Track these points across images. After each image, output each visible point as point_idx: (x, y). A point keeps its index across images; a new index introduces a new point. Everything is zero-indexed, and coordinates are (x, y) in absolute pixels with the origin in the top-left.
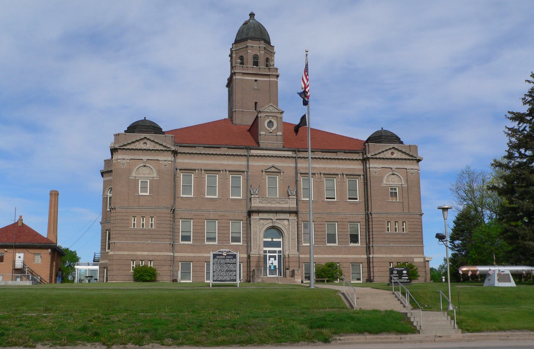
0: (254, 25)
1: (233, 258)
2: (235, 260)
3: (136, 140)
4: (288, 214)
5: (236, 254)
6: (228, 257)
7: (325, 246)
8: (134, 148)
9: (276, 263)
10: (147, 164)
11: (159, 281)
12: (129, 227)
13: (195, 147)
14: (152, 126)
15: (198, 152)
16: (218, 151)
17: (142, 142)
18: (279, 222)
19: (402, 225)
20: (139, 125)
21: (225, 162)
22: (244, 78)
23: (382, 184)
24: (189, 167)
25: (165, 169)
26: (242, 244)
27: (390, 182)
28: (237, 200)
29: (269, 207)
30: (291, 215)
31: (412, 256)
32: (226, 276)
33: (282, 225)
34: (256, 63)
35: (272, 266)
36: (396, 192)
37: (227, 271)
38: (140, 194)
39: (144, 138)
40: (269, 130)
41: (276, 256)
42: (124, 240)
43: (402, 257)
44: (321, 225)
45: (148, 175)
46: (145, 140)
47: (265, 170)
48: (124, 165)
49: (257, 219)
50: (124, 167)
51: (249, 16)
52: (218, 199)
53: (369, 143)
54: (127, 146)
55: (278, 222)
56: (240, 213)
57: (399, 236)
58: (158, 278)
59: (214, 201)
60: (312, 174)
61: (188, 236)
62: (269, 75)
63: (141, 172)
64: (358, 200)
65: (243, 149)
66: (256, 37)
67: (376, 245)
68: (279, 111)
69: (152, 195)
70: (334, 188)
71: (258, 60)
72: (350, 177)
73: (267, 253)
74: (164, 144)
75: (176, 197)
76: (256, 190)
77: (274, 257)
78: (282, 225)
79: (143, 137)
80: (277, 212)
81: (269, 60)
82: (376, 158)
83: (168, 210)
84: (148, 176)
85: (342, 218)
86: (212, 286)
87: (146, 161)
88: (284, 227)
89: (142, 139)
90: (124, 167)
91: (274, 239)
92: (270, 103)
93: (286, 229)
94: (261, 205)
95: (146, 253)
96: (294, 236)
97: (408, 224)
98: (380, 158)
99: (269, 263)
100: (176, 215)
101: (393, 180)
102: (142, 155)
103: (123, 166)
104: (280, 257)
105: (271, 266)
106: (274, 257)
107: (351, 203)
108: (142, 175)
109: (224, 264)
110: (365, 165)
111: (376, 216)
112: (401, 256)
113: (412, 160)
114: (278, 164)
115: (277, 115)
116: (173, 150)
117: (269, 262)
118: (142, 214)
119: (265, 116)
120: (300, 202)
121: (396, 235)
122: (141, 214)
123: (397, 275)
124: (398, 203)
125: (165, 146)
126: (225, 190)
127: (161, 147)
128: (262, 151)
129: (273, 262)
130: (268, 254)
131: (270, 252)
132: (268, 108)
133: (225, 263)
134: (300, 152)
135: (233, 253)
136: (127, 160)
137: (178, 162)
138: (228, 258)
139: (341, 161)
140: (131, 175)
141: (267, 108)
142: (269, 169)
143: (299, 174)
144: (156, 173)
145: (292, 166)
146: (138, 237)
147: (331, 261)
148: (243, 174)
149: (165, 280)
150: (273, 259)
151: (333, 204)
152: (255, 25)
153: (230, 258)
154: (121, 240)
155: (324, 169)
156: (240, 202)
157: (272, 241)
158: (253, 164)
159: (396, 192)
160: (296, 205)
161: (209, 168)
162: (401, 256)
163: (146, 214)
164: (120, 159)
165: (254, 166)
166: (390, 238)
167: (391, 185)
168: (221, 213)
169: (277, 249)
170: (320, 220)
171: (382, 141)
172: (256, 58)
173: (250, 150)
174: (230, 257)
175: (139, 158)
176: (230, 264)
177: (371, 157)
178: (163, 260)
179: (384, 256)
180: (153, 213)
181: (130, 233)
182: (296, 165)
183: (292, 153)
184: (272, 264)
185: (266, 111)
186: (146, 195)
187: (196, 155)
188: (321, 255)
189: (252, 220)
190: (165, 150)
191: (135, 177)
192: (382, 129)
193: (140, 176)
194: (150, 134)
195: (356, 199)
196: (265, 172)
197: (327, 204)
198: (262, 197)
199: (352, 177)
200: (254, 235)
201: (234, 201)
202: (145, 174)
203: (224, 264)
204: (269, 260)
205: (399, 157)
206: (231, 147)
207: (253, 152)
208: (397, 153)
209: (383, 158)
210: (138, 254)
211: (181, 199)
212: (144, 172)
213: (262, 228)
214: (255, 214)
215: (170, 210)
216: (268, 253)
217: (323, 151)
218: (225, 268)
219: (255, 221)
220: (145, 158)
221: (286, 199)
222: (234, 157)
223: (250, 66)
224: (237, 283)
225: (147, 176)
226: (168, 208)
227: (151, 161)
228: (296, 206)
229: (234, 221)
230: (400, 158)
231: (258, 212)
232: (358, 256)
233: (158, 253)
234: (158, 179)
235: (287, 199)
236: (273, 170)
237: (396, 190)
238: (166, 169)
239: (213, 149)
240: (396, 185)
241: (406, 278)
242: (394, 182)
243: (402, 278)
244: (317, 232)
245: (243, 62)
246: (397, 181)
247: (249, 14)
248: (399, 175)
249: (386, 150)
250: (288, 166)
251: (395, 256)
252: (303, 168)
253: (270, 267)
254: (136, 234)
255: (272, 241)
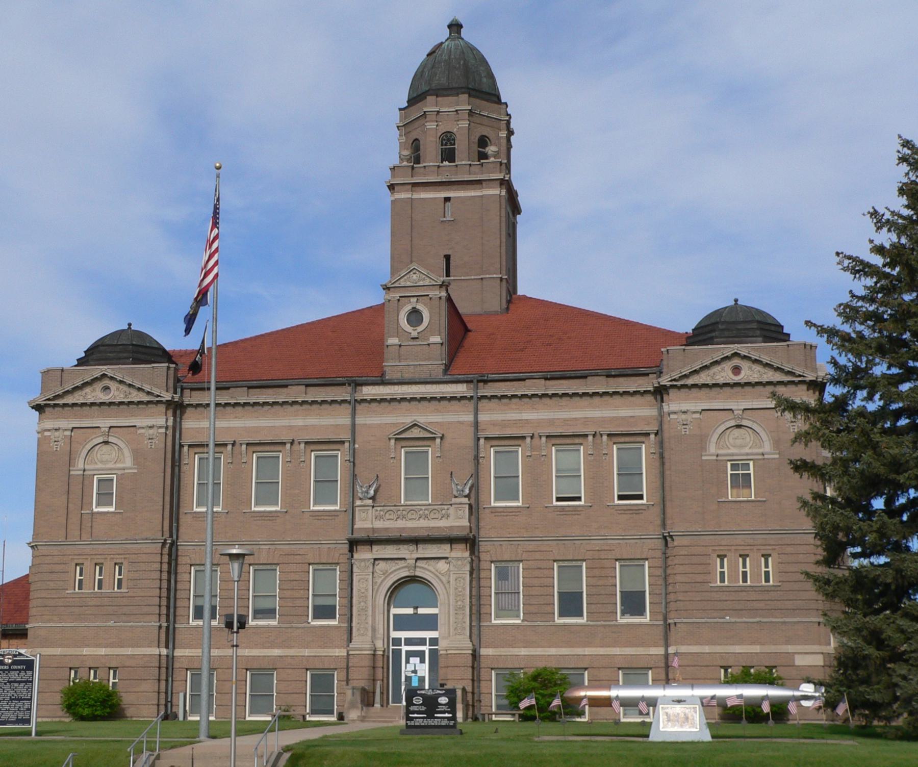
0: (450, 56)
1: (25, 670)
2: (29, 673)
3: (703, 367)
4: (447, 544)
5: (33, 660)
6: (15, 667)
7: (551, 623)
8: (710, 382)
9: (424, 670)
10: (743, 420)
11: (131, 717)
12: (67, 589)
13: (228, 388)
14: (133, 345)
15: (233, 401)
16: (281, 396)
17: (99, 386)
18: (426, 566)
19: (84, 583)
20: (103, 345)
21: (299, 422)
22: (415, 196)
23: (703, 454)
24: (269, 439)
25: (149, 447)
26: (337, 623)
27: (729, 448)
28: (328, 514)
29: (400, 528)
30: (454, 546)
31: (790, 648)
32: (9, 710)
33: (433, 573)
34: (449, 155)
35: (413, 678)
36: (750, 474)
37: (11, 699)
38: (95, 510)
39: (102, 375)
40: (410, 333)
41: (424, 652)
42: (54, 621)
43: (758, 651)
44: (540, 569)
45: (113, 462)
46: (107, 382)
47: (395, 435)
48: (153, 441)
49: (369, 560)
50: (59, 446)
51: (448, 30)
52: (279, 514)
53: (669, 348)
54: (65, 397)
55: (423, 565)
56: (333, 546)
57: (753, 596)
58: (129, 713)
59: (271, 518)
60: (216, 445)
61: (330, 606)
62: (479, 182)
63: (731, 440)
64: (644, 501)
65: (344, 384)
66: (451, 86)
67: (685, 620)
68: (437, 282)
69: (122, 511)
70: (579, 470)
71: (454, 144)
72: (623, 439)
73: (401, 645)
74: (147, 388)
75: (181, 513)
76: (370, 486)
77: (421, 655)
78: (433, 573)
79: (729, 354)
80: (416, 541)
81: (490, 141)
82: (55, 405)
83: (156, 545)
84: (750, 451)
85: (598, 550)
86: (37, 734)
87: (740, 412)
88: (437, 576)
89: (727, 358)
90: (59, 446)
91: (419, 609)
92: (412, 262)
93: (442, 582)
94: (379, 524)
95: (102, 651)
96: (365, 603)
97: (780, 560)
98: (695, 386)
99: (406, 669)
100: (182, 556)
101: (738, 442)
102: (98, 417)
103: (150, 444)
104: (434, 654)
105: (411, 677)
106: (421, 655)
107: (625, 508)
108: (100, 466)
109: (5, 684)
110: (178, 420)
111: (685, 541)
112: (757, 649)
113: (792, 382)
114: (428, 417)
115: (431, 293)
116: (811, 381)
117: (406, 668)
118: (115, 556)
119: (400, 297)
120: (487, 511)
121: (741, 591)
122: (93, 559)
123: (424, 708)
124: (753, 504)
125: (789, 373)
126: (299, 491)
127: (778, 375)
128: (450, 385)
129: (417, 669)
130: (405, 648)
131: (409, 642)
132: (408, 276)
133: (8, 682)
134: (490, 384)
135: (27, 657)
136: (66, 430)
137: (186, 427)
138: (15, 670)
139: (597, 399)
140: (74, 467)
141: (405, 277)
142: (408, 432)
143: (482, 441)
144: (768, 442)
145: (466, 419)
146: (87, 612)
147: (541, 665)
148: (341, 449)
149: (145, 715)
150: (418, 659)
151: (575, 515)
152: (453, 53)
153: (20, 670)
154: (49, 621)
155: (551, 422)
156: (333, 517)
157: (416, 614)
158: (368, 422)
159: (750, 474)
160: (467, 520)
161: (256, 439)
162: (757, 649)
163: (106, 556)
164: (675, 413)
165: (369, 426)
166: (726, 601)
167: (733, 455)
168: (287, 547)
169: (428, 635)
170: (537, 556)
171: (712, 338)
172: (449, 140)
173: (360, 388)
174: (19, 667)
175: (127, 425)
176: (20, 682)
177: (671, 383)
178: (142, 667)
179: (707, 649)
180: (122, 554)
181: (68, 604)
182: (355, 421)
183: (467, 388)
184: (415, 672)
185: (403, 284)
186: (108, 513)
187: (229, 409)
188: (540, 649)
189: (356, 563)
190: (789, 381)
191: (717, 456)
192: (129, 328)
193: (730, 451)
194: (117, 366)
195: (640, 497)
196: (397, 439)
197: (557, 515)
198: (383, 504)
199: (627, 439)
200: (361, 600)
201: (320, 518)
202: (107, 462)
203: (5, 684)
204: (407, 662)
205: (755, 378)
206: (280, 384)
207: (368, 391)
208: (750, 368)
209: (706, 386)
210: (84, 654)
211: (193, 517)
212: (105, 457)
213: (382, 581)
214: (363, 547)
215: (161, 544)
216: (406, 644)
217: (549, 377)
218: (8, 692)
219: (363, 564)
220: (104, 423)
221: (443, 507)
222: (321, 407)
223: (431, 164)
224: (32, 727)
225: (110, 465)
226: (153, 541)
227: (119, 429)
228: (468, 524)
229: (321, 567)
230: (126, 400)
231: (370, 542)
232: (640, 651)
233: (129, 651)
234: (136, 471)
235: (446, 507)
236: (416, 433)
237: (749, 470)
238: (153, 447)
239: (270, 391)
240: (747, 454)
241: (447, 715)
242: (741, 446)
243: (436, 715)
244: (530, 589)
245: (419, 154)
246: (750, 445)
247: (447, 24)
248: (755, 427)
249: (716, 363)
250: (456, 420)
251: (738, 649)
252: (494, 424)
253: (408, 679)
254: (82, 606)
255: (416, 614)
